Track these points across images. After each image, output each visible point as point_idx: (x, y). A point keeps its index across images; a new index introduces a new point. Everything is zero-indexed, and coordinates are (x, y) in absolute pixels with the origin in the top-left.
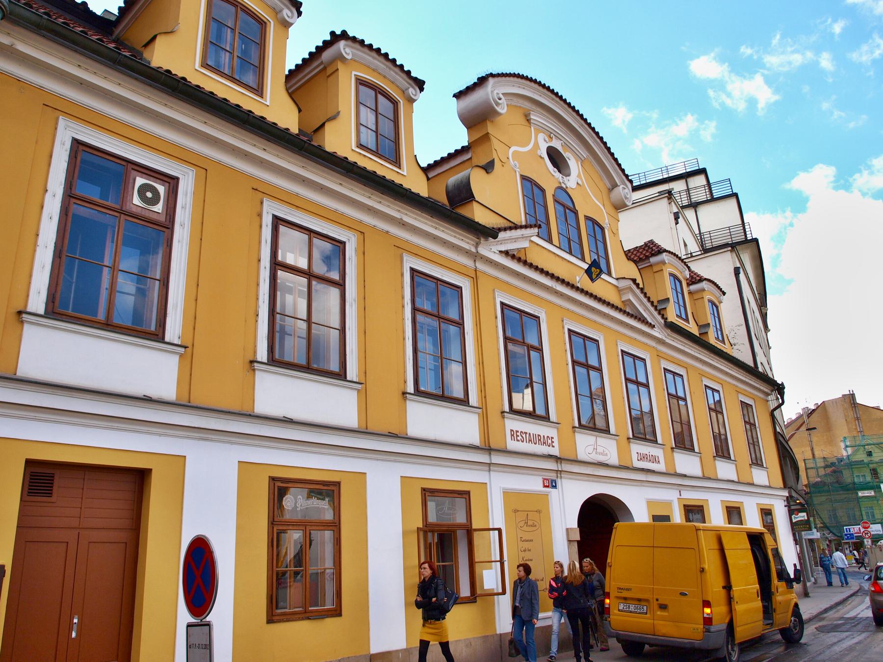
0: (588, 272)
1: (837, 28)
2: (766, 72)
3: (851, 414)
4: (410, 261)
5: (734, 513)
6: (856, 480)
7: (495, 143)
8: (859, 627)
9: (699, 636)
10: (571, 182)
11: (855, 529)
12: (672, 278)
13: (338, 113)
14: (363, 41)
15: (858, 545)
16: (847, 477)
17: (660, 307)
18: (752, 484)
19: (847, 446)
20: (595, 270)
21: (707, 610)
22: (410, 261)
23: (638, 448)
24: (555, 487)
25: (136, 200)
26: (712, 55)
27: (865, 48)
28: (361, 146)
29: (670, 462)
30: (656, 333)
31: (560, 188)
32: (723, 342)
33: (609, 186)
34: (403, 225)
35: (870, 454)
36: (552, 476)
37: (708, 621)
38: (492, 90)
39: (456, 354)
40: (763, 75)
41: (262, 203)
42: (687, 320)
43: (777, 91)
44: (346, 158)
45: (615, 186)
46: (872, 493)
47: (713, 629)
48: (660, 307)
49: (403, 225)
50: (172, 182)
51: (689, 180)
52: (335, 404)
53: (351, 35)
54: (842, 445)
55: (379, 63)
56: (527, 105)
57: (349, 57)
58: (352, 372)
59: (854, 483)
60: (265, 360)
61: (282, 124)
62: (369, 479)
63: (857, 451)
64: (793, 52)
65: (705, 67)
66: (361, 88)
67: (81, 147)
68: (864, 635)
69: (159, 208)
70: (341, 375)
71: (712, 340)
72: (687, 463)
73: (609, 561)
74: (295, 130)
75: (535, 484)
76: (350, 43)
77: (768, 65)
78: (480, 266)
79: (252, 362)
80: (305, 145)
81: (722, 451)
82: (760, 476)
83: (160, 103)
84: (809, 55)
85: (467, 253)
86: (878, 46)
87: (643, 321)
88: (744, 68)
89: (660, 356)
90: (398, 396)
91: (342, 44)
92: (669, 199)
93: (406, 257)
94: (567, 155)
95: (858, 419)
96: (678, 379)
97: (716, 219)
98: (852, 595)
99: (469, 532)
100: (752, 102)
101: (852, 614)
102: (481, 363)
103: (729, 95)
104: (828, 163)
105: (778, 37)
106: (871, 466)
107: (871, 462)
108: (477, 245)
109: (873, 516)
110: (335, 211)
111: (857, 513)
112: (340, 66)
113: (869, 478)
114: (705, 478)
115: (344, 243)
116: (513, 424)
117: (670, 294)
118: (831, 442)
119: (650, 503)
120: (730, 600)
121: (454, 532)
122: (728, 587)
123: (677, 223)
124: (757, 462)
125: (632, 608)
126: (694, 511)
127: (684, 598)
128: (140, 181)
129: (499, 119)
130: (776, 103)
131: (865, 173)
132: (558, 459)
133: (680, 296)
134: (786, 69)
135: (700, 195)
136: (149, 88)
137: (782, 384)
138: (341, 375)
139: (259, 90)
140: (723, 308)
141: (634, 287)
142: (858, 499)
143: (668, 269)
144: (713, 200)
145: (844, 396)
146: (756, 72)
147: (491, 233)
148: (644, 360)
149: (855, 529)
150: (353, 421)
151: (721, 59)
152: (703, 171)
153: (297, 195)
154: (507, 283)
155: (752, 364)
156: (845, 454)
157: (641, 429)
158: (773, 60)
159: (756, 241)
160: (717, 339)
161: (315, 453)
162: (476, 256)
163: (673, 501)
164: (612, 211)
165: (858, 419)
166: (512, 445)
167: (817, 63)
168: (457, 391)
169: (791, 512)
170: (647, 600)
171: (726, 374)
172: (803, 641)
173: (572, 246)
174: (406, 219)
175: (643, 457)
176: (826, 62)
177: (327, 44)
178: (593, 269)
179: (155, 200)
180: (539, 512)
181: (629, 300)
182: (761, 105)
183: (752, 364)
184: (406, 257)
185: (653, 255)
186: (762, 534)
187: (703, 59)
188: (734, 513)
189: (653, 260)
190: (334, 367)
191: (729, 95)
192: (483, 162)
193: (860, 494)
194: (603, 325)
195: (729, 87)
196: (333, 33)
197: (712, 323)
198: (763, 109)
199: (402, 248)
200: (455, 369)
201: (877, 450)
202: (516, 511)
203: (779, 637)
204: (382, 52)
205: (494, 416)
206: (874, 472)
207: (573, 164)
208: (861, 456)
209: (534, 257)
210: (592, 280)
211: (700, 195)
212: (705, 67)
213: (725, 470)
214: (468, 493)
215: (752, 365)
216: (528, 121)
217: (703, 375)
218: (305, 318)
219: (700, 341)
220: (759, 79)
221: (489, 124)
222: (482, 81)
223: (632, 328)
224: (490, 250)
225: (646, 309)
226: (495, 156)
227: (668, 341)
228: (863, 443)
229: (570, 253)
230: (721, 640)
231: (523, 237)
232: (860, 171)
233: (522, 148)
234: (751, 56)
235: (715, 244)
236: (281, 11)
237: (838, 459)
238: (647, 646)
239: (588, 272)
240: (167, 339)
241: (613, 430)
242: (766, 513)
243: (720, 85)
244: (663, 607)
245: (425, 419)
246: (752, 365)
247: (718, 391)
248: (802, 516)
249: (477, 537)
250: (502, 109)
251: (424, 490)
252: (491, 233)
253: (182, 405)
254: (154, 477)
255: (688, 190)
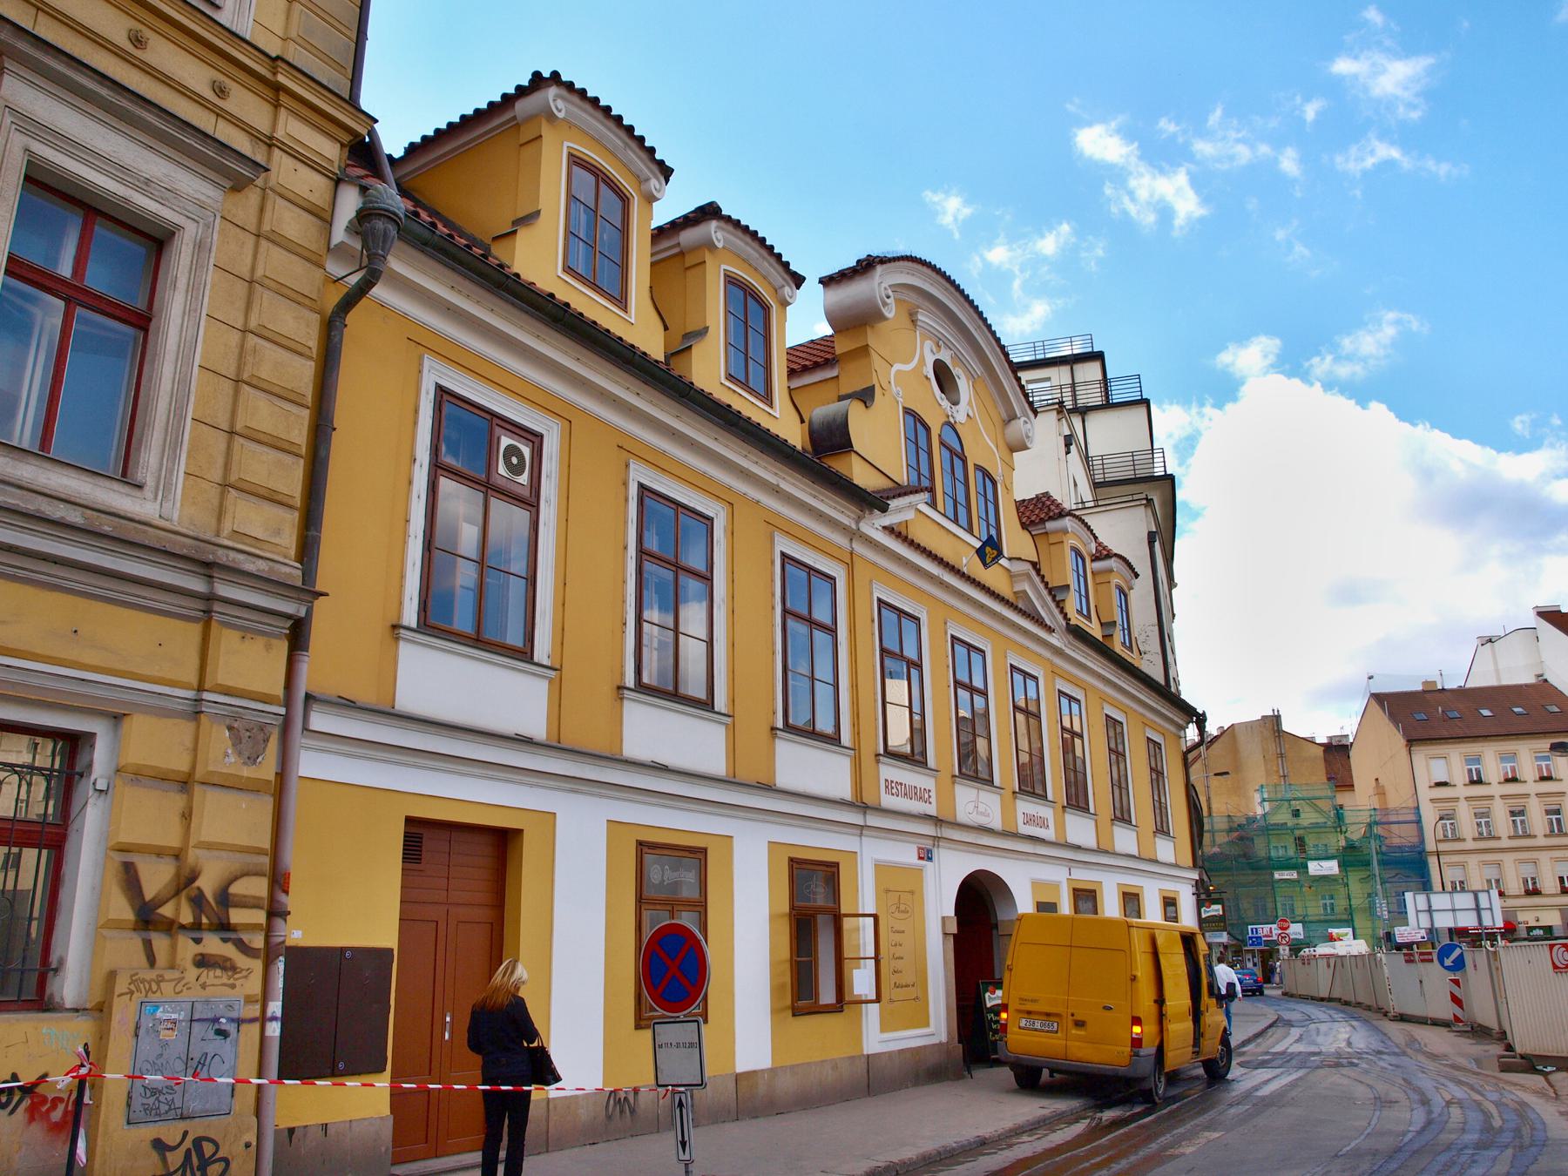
0: (980, 552)
1: (1310, 112)
2: (1192, 167)
3: (1272, 747)
4: (640, 474)
5: (1131, 900)
6: (1273, 854)
7: (877, 362)
8: (1294, 1062)
9: (1127, 1061)
10: (960, 415)
11: (1264, 930)
12: (910, 420)
13: (538, 213)
14: (764, 239)
15: (1268, 955)
16: (1260, 848)
17: (1056, 593)
18: (1156, 861)
19: (1264, 800)
20: (990, 550)
21: (1137, 1029)
22: (640, 474)
23: (1026, 806)
24: (930, 859)
25: (502, 470)
26: (1113, 125)
27: (1353, 150)
28: (568, 269)
29: (1060, 826)
30: (1054, 640)
31: (948, 424)
32: (1088, 617)
33: (1005, 416)
34: (776, 491)
35: (1296, 814)
36: (928, 844)
37: (1137, 1042)
38: (879, 284)
39: (823, 671)
40: (1188, 173)
41: (627, 466)
42: (1088, 617)
43: (1205, 200)
44: (552, 295)
45: (1012, 417)
46: (1294, 875)
47: (1143, 1052)
48: (1056, 593)
49: (776, 491)
50: (535, 439)
51: (1076, 367)
52: (511, 699)
53: (564, 79)
54: (1257, 797)
55: (752, 251)
56: (913, 298)
57: (561, 115)
58: (542, 651)
59: (1270, 858)
60: (414, 625)
61: (791, 442)
62: (737, 846)
63: (1279, 807)
64: (1238, 141)
65: (1099, 143)
66: (576, 169)
67: (446, 397)
68: (1301, 1073)
69: (524, 479)
70: (523, 654)
71: (1118, 648)
72: (1080, 830)
73: (1009, 962)
74: (799, 447)
75: (905, 854)
76: (722, 224)
77: (1198, 157)
78: (859, 548)
79: (395, 627)
80: (664, 379)
81: (1122, 816)
82: (1165, 850)
83: (532, 334)
84: (1264, 149)
85: (845, 530)
86: (1372, 152)
87: (1039, 622)
88: (1161, 155)
89: (1055, 672)
90: (607, 689)
91: (552, 91)
92: (1059, 412)
93: (428, 362)
94: (957, 371)
95: (1281, 755)
96: (975, 657)
97: (1109, 436)
98: (1271, 1026)
99: (837, 919)
100: (1165, 212)
101: (1278, 1048)
102: (854, 686)
103: (1131, 194)
104: (1271, 333)
105: (1218, 112)
106: (1297, 833)
107: (1297, 826)
108: (858, 520)
109: (1293, 910)
110: (703, 475)
111: (1270, 905)
112: (546, 131)
113: (1291, 852)
114: (1100, 851)
115: (711, 520)
116: (890, 772)
117: (1071, 580)
118: (1239, 790)
119: (1037, 885)
120: (1161, 1016)
121: (814, 916)
122: (1160, 1001)
123: (1068, 452)
124: (1162, 830)
125: (1038, 1025)
126: (1085, 897)
127: (1108, 1013)
128: (506, 441)
129: (882, 326)
130: (1201, 220)
131: (1329, 358)
132: (937, 821)
133: (923, 457)
134: (1225, 167)
135: (1092, 396)
136: (524, 316)
137: (1204, 714)
138: (707, 705)
139: (622, 301)
140: (1133, 595)
141: (1033, 573)
142: (1273, 883)
143: (1071, 541)
144: (1108, 405)
145: (1264, 717)
146: (1180, 165)
147: (872, 502)
148: (918, 619)
149: (1264, 930)
150: (719, 767)
151: (1127, 134)
152: (1098, 356)
153: (664, 453)
154: (886, 570)
155: (1162, 681)
156: (1259, 811)
157: (1030, 783)
158: (1203, 148)
159: (1169, 479)
160: (1080, 612)
161: (360, 757)
162: (854, 534)
163: (1060, 879)
164: (1005, 452)
165: (1281, 755)
166: (888, 801)
167: (1275, 161)
168: (824, 725)
169: (1200, 904)
170: (1058, 1015)
171: (1134, 698)
172: (1229, 1076)
173: (959, 513)
174: (784, 486)
175: (1030, 820)
176: (1289, 163)
177: (521, 91)
178: (988, 549)
179: (517, 470)
180: (912, 893)
181: (1025, 592)
182: (1179, 221)
183: (1162, 681)
184: (428, 362)
185: (1051, 518)
186: (1193, 934)
187: (1098, 130)
188: (1131, 900)
189: (1050, 525)
190: (515, 638)
191: (1133, 199)
192: (859, 386)
193: (1277, 876)
194: (957, 610)
195: (1133, 183)
196: (537, 76)
197: (1074, 586)
198: (1181, 228)
199: (628, 450)
200: (823, 692)
201: (1307, 809)
202: (887, 891)
203: (1201, 1071)
204: (614, 113)
205: (867, 759)
206: (1300, 842)
207: (964, 385)
208: (1283, 817)
209: (921, 534)
210: (985, 565)
211: (1092, 396)
212: (1099, 143)
213: (1125, 840)
214: (704, 851)
215: (1162, 682)
216: (914, 322)
217: (775, 525)
218: (474, 555)
219: (1102, 649)
220: (1181, 179)
221: (869, 330)
222: (866, 266)
223: (1026, 632)
224: (874, 526)
225: (1045, 604)
226: (875, 382)
227: (1068, 651)
228: (1289, 796)
229: (956, 521)
230: (1146, 1067)
231: (910, 506)
232: (1318, 353)
233: (903, 364)
234: (1174, 137)
235: (1110, 477)
236: (648, 180)
237: (1248, 819)
238: (1045, 1072)
239: (980, 552)
240: (536, 659)
241: (997, 781)
242: (1170, 903)
243: (1117, 175)
244: (1080, 1024)
245: (651, 731)
246: (1162, 682)
247: (1078, 701)
248: (1216, 909)
249: (847, 923)
250: (890, 313)
251: (640, 844)
252: (872, 502)
253: (553, 747)
254: (526, 835)
255: (1073, 385)
